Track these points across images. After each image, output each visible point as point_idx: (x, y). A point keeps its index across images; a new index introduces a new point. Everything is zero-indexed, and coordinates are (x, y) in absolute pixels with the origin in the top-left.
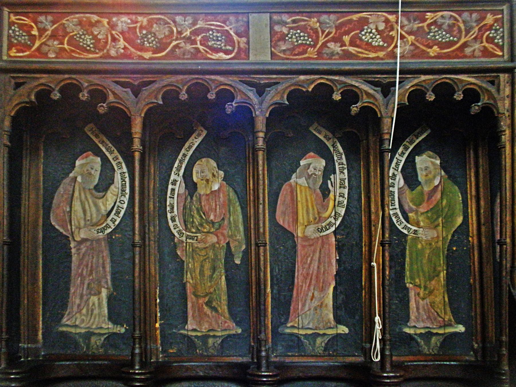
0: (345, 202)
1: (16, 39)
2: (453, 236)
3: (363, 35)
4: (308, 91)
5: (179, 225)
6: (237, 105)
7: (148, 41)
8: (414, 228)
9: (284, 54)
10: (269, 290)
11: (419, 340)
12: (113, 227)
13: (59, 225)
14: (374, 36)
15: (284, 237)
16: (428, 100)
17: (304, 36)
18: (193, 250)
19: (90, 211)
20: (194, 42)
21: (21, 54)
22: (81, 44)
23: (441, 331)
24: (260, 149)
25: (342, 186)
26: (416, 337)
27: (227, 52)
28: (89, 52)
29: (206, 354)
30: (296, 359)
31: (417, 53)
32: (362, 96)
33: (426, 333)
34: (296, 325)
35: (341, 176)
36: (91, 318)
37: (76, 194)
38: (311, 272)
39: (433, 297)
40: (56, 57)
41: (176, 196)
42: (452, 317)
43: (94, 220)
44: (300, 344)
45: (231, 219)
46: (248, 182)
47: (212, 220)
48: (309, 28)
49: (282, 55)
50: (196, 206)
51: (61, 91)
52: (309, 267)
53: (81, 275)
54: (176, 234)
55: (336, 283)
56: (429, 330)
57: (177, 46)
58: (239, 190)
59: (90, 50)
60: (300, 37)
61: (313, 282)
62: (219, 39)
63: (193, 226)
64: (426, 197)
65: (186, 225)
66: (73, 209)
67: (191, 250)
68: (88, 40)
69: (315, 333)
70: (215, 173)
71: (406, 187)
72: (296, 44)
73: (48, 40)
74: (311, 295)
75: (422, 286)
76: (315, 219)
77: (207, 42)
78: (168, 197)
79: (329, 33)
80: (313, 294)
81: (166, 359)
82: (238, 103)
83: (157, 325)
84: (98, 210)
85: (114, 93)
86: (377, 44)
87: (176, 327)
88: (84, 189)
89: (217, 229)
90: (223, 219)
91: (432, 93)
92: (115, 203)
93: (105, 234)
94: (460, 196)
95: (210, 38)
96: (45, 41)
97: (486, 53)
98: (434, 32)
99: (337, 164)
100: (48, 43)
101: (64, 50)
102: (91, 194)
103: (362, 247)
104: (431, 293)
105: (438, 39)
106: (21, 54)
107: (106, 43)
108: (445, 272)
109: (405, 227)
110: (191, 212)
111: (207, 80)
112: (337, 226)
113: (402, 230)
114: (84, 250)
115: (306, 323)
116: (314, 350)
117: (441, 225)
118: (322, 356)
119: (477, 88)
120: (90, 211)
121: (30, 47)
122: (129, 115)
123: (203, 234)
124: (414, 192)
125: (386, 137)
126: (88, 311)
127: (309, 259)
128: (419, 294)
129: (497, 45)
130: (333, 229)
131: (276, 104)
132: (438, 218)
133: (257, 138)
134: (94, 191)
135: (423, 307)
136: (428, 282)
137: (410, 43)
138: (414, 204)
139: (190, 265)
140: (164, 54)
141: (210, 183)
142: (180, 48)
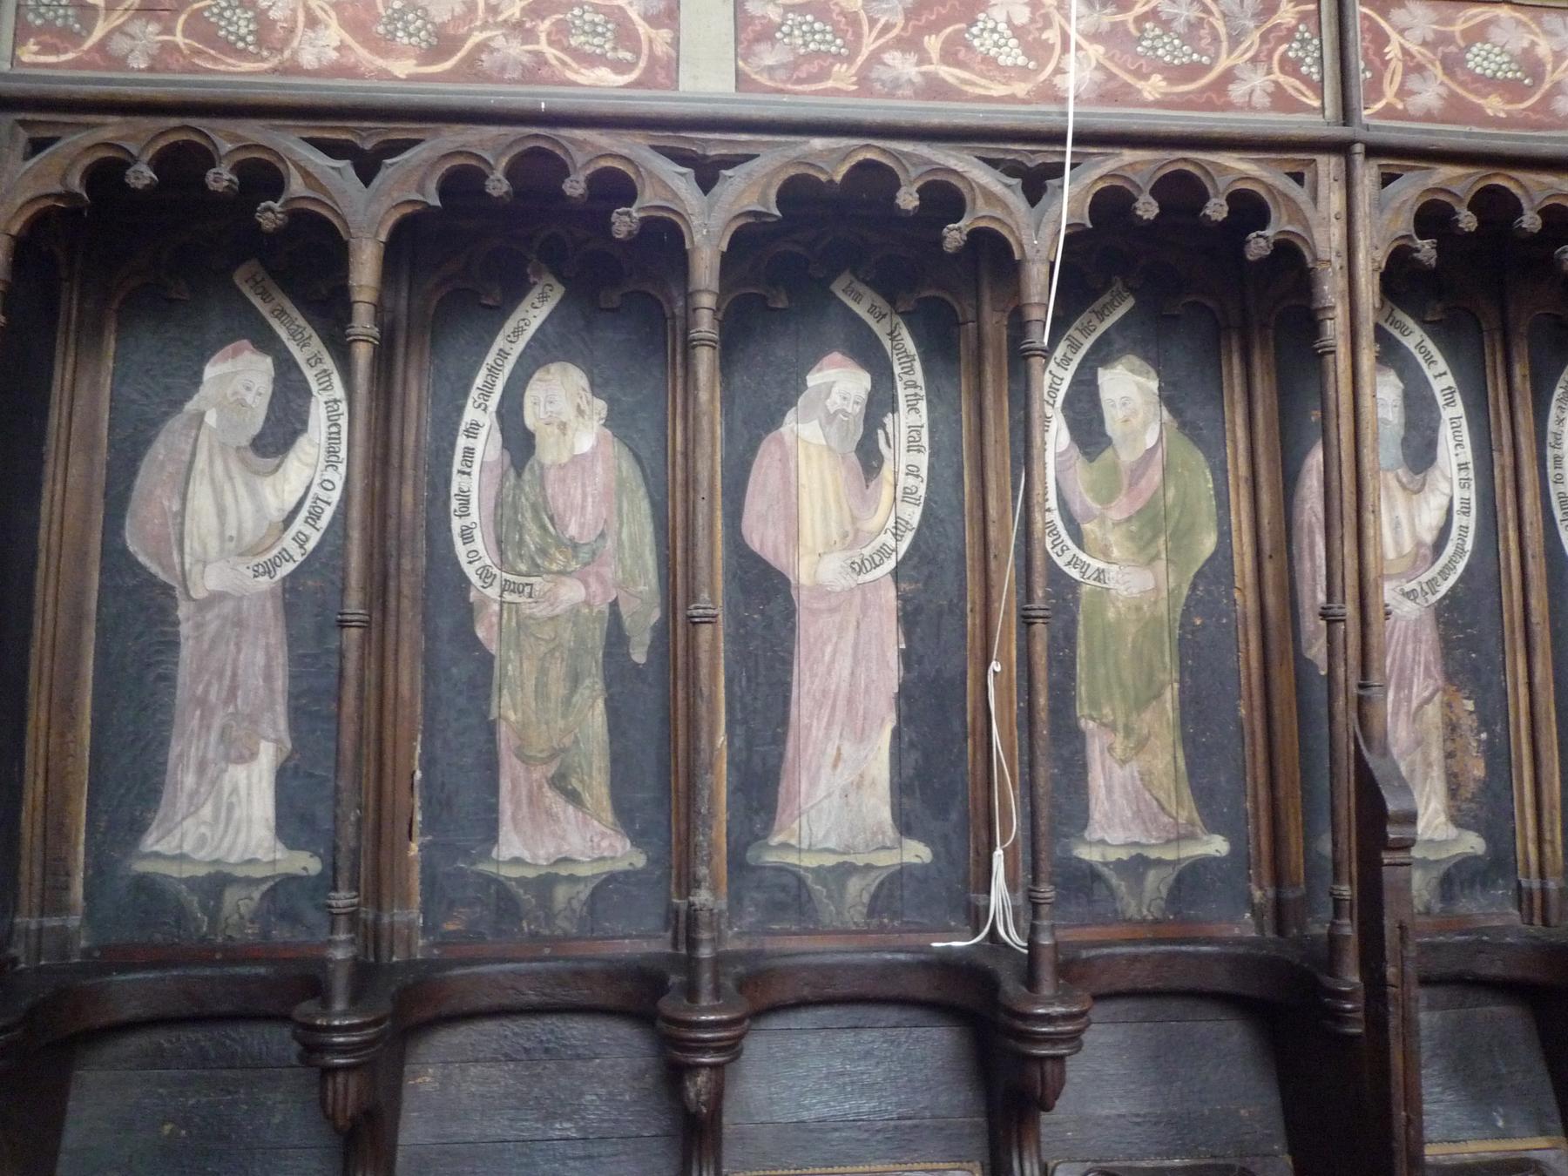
0: (922, 491)
1: (40, 15)
2: (1194, 587)
3: (975, 36)
4: (831, 181)
5: (482, 552)
6: (643, 214)
7: (405, 29)
8: (1096, 564)
9: (771, 78)
10: (721, 739)
11: (1114, 881)
12: (299, 559)
13: (147, 554)
14: (1002, 41)
15: (765, 591)
16: (1141, 217)
17: (823, 32)
18: (518, 623)
19: (238, 512)
20: (529, 36)
21: (52, 59)
22: (222, 33)
23: (1169, 855)
24: (702, 342)
25: (913, 447)
26: (1105, 871)
27: (619, 67)
28: (243, 54)
29: (546, 932)
30: (792, 944)
31: (1111, 93)
32: (974, 201)
33: (1132, 858)
34: (793, 842)
35: (911, 419)
36: (226, 831)
37: (201, 462)
38: (833, 687)
39: (1148, 757)
40: (151, 69)
41: (475, 469)
42: (1196, 815)
43: (248, 539)
44: (804, 897)
45: (624, 536)
46: (670, 432)
47: (572, 539)
48: (837, 10)
49: (763, 79)
50: (532, 498)
51: (158, 163)
52: (829, 673)
53: (202, 702)
54: (474, 578)
55: (899, 717)
56: (1139, 851)
57: (482, 47)
58: (645, 453)
59: (244, 50)
60: (814, 33)
61: (840, 715)
62: (600, 29)
63: (521, 556)
64: (1125, 482)
65: (501, 553)
66: (189, 505)
67: (514, 624)
68: (242, 23)
69: (845, 863)
70: (584, 406)
71: (1075, 452)
72: (802, 51)
73: (131, 19)
74: (835, 752)
75: (1120, 726)
76: (845, 535)
77: (566, 37)
78: (455, 471)
79: (887, 28)
80: (839, 749)
81: (436, 952)
82: (643, 209)
83: (414, 848)
84: (259, 509)
85: (306, 175)
86: (1009, 62)
87: (466, 853)
88: (223, 446)
89: (586, 564)
90: (602, 535)
91: (1151, 200)
92: (308, 488)
93: (278, 577)
94: (1209, 477)
95: (576, 27)
96: (124, 24)
97: (1281, 100)
98: (1153, 39)
99: (900, 385)
100: (129, 29)
101: (176, 47)
102: (243, 461)
103: (964, 616)
104: (1141, 745)
105: (1161, 57)
106: (52, 59)
107: (292, 31)
108: (1176, 686)
109: (1073, 562)
110: (516, 513)
111: (564, 143)
112: (900, 556)
113: (1066, 569)
114: (212, 627)
115: (820, 836)
116: (839, 913)
117: (1163, 556)
118: (866, 932)
119: (1262, 192)
120: (238, 512)
121: (75, 39)
122: (345, 237)
123: (549, 577)
124: (1095, 464)
125: (1035, 314)
126: (217, 810)
127: (829, 649)
128: (1111, 749)
129: (1306, 80)
130: (890, 564)
131: (749, 213)
132: (1155, 537)
133: (695, 310)
134: (250, 455)
135: (1124, 786)
136: (1134, 715)
137: (1094, 64)
138: (1096, 499)
139: (510, 667)
140: (448, 65)
141: (569, 432)
142: (492, 51)
